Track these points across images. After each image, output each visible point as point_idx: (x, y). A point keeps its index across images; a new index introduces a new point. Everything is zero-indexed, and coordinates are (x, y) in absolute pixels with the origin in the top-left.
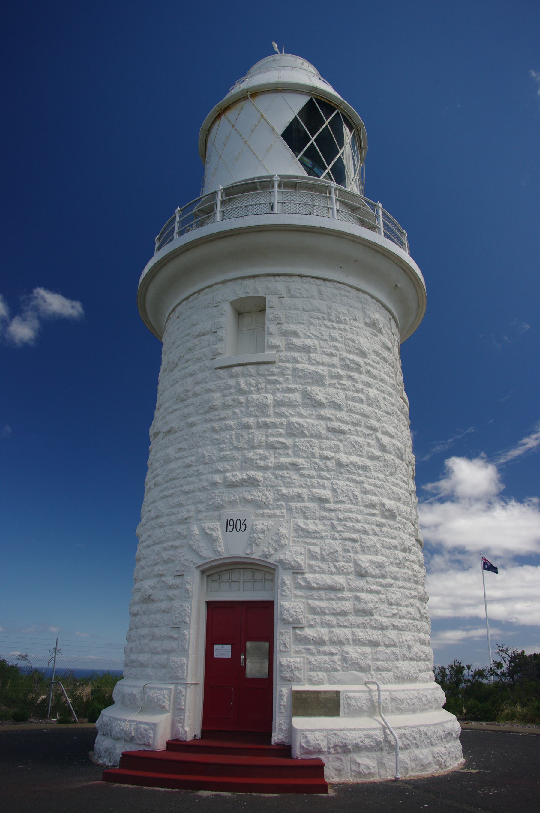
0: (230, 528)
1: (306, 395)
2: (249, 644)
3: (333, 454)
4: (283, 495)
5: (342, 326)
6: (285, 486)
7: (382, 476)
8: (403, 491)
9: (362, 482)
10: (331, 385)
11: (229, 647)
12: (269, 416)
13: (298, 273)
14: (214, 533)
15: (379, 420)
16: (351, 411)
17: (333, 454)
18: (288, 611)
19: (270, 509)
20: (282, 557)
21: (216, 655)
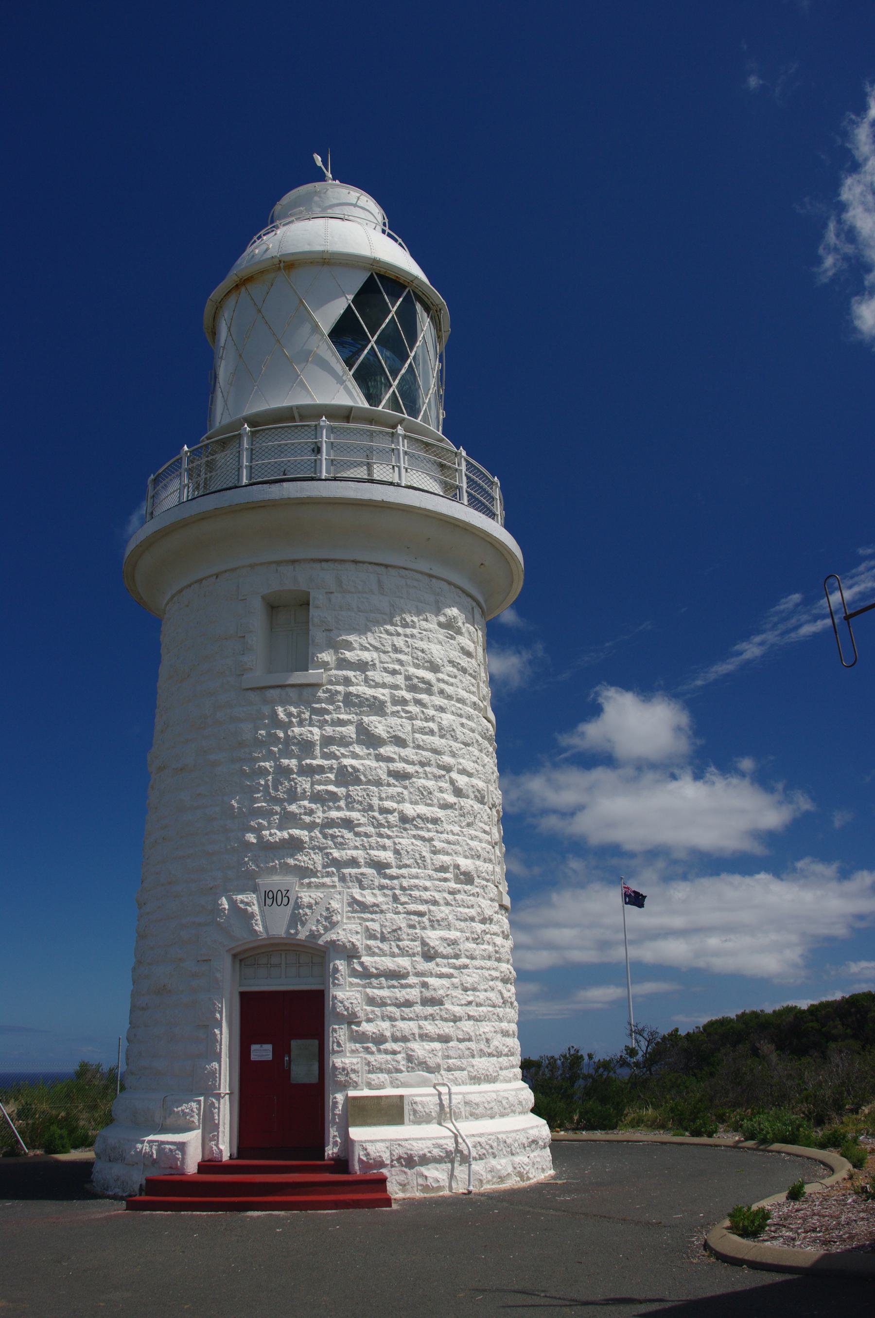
0: (269, 902)
3: (395, 805)
5: (408, 631)
6: (336, 848)
7: (456, 829)
8: (484, 845)
9: (431, 840)
10: (395, 714)
11: (269, 1047)
12: (314, 759)
15: (453, 755)
16: (419, 747)
17: (395, 805)
19: (318, 877)
20: (334, 937)
21: (254, 1057)
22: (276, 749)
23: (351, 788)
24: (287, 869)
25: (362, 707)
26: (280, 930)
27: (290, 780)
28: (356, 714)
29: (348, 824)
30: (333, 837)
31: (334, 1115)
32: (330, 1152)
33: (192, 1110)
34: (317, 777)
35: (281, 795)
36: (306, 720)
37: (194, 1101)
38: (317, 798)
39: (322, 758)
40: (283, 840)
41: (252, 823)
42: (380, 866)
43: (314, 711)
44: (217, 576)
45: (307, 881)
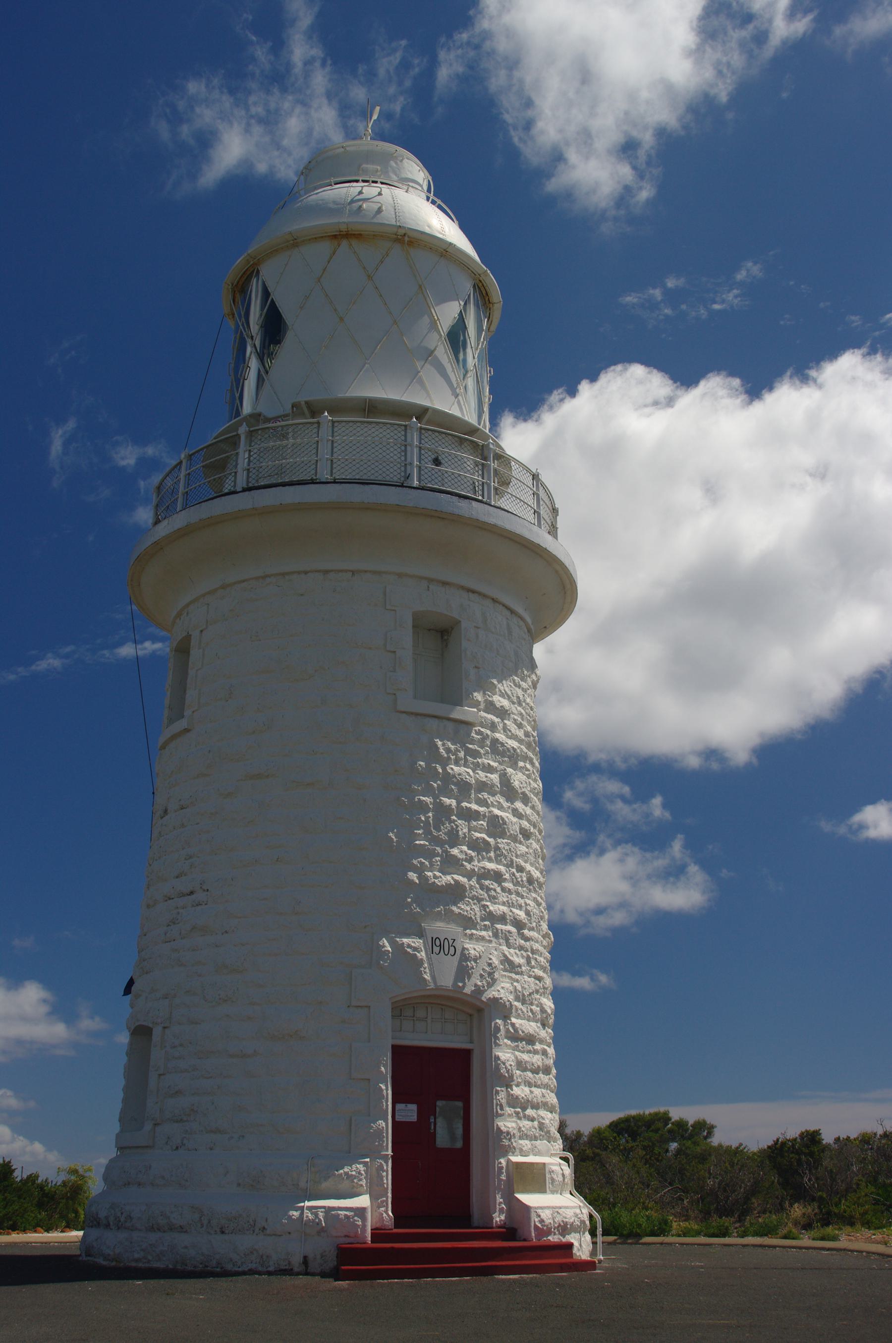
0: (436, 949)
1: (505, 781)
2: (439, 1103)
4: (490, 913)
6: (490, 901)
11: (413, 1107)
13: (495, 597)
14: (418, 954)
18: (504, 1064)
19: (477, 930)
20: (496, 995)
22: (435, 785)
23: (499, 840)
24: (450, 917)
25: (505, 757)
26: (447, 981)
27: (451, 821)
28: (499, 762)
29: (498, 877)
30: (488, 889)
31: (500, 1180)
32: (498, 1219)
33: (359, 1173)
34: (475, 823)
35: (444, 837)
36: (461, 759)
37: (360, 1163)
38: (475, 845)
39: (476, 803)
40: (449, 885)
41: (415, 862)
42: (519, 925)
43: (468, 752)
44: (353, 572)
45: (468, 932)
